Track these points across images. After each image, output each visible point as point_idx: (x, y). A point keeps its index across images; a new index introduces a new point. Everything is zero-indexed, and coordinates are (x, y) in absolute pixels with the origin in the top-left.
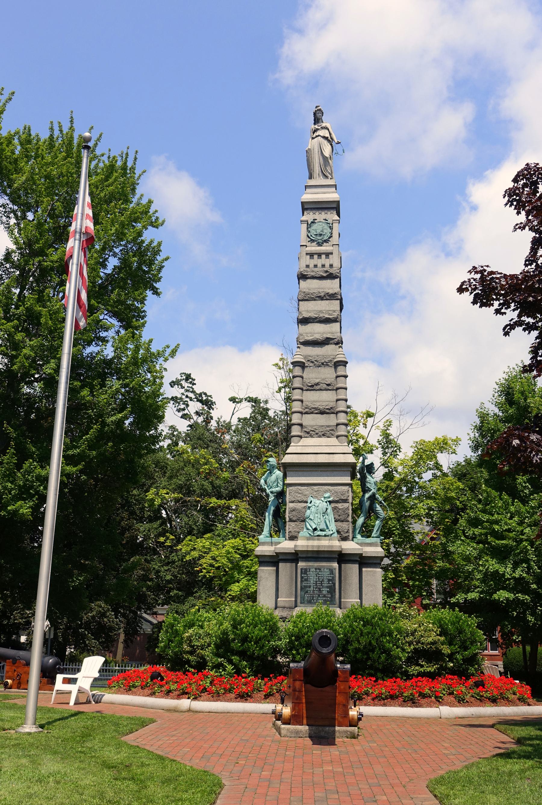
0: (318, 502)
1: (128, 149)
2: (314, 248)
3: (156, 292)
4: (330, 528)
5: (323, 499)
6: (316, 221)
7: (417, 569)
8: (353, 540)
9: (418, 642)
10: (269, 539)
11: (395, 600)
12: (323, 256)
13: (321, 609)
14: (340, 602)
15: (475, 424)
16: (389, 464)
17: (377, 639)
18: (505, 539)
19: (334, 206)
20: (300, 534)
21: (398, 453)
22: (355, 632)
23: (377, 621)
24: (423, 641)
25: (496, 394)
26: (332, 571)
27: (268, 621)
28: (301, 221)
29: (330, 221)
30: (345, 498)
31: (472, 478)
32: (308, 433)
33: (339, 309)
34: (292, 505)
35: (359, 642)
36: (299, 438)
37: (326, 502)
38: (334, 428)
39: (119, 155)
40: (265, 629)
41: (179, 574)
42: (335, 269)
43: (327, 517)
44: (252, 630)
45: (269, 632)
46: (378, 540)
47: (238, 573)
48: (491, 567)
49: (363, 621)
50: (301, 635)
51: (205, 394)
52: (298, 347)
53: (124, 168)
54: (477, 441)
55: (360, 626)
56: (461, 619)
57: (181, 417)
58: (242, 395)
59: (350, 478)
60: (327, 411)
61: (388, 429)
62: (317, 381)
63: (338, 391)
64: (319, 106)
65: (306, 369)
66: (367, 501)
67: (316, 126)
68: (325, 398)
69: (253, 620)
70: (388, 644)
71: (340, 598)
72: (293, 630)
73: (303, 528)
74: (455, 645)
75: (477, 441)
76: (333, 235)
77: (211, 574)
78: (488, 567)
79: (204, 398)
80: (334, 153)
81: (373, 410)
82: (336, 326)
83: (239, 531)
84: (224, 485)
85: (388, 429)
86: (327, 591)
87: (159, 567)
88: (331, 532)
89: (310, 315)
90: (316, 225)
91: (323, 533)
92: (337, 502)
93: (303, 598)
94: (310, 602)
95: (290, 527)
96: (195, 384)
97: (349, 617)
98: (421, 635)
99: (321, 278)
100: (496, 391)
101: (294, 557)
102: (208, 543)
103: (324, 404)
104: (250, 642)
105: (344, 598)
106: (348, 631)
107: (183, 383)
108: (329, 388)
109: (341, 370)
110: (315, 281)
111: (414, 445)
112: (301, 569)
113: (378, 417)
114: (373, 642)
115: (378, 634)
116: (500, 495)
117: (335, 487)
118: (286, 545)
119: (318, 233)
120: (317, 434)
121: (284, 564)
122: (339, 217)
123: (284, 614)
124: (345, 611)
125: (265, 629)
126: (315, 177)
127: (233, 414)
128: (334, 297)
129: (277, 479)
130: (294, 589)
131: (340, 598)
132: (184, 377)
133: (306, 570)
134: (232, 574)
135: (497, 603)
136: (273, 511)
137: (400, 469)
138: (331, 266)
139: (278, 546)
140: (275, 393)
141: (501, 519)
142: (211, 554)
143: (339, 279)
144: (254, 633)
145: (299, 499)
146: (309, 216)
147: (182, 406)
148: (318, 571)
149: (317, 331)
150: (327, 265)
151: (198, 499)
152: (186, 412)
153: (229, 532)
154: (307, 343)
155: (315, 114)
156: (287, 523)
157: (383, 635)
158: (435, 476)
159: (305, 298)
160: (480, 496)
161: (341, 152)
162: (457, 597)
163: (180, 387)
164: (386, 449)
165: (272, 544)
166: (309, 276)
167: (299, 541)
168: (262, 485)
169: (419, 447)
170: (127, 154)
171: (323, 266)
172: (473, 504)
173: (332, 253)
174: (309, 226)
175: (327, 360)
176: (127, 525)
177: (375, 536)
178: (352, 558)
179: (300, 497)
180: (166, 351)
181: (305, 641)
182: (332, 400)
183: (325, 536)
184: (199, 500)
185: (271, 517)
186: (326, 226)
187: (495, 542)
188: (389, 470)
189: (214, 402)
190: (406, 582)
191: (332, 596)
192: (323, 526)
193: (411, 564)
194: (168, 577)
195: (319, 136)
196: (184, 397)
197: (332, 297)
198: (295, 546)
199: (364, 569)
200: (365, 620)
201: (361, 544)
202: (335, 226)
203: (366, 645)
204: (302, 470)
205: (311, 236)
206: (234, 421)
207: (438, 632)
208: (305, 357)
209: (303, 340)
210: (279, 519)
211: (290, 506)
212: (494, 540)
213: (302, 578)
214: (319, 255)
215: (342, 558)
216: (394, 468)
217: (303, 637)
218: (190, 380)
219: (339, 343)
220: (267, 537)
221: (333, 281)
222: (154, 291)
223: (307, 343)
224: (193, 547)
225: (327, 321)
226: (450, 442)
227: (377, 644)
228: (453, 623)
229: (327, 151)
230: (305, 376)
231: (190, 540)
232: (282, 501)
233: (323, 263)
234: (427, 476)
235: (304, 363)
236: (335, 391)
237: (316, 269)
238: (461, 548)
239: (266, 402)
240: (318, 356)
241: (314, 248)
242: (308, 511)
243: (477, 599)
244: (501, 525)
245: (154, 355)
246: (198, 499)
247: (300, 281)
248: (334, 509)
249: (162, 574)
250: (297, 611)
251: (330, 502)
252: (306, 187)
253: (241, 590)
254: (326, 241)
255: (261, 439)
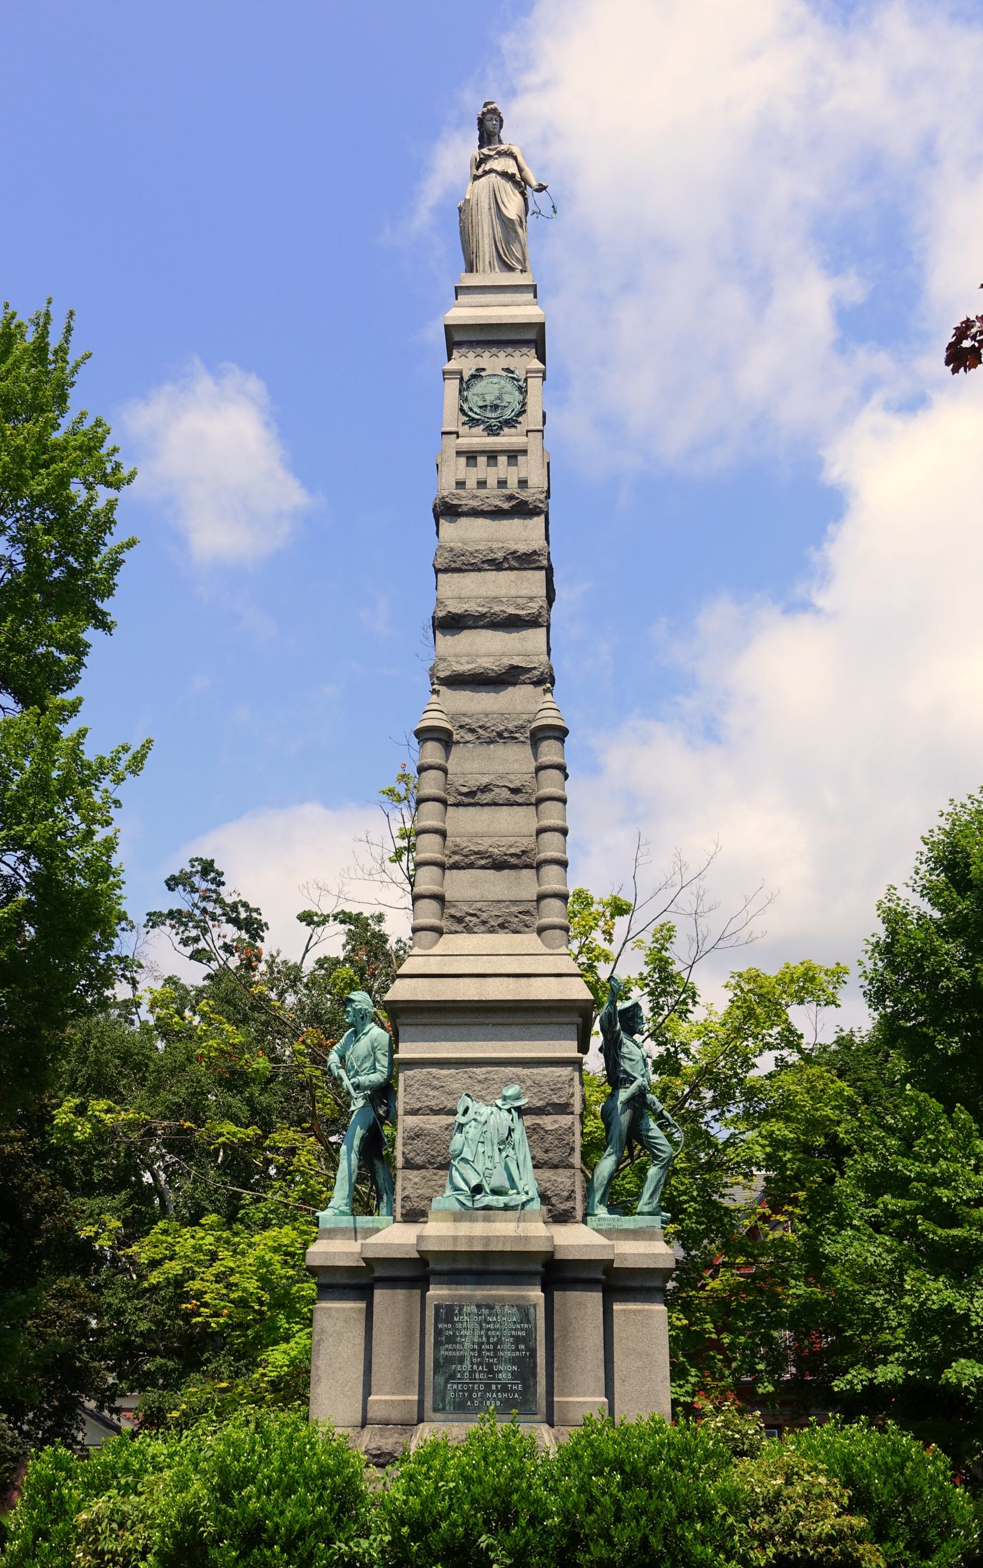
0: (485, 1110)
1: (49, 303)
2: (477, 439)
3: (103, 623)
4: (520, 1184)
5: (499, 1102)
6: (483, 374)
7: (739, 1305)
8: (584, 1222)
9: (789, 1535)
10: (347, 1221)
11: (688, 1387)
12: (502, 460)
13: (493, 1433)
14: (550, 1404)
15: (874, 940)
16: (669, 1035)
17: (665, 1530)
18: (962, 1227)
19: (532, 336)
20: (435, 1204)
21: (690, 1007)
22: (598, 1509)
23: (663, 1472)
24: (805, 1532)
25: (924, 868)
26: (525, 1313)
27: (330, 1474)
28: (444, 373)
29: (520, 374)
30: (563, 1100)
31: (860, 1079)
32: (460, 920)
33: (543, 592)
34: (411, 1121)
35: (609, 1540)
36: (434, 934)
37: (509, 1111)
38: (531, 907)
39: (31, 321)
40: (320, 1500)
41: (168, 1317)
42: (532, 491)
43: (511, 1153)
44: (276, 1505)
45: (330, 1510)
46: (656, 1221)
47: (288, 1318)
48: (934, 1297)
49: (622, 1472)
50: (428, 1519)
51: (245, 905)
52: (434, 692)
53: (41, 348)
54: (881, 981)
55: (614, 1489)
56: (909, 1458)
57: (191, 957)
58: (328, 907)
59: (575, 1044)
60: (513, 860)
61: (663, 948)
62: (485, 780)
63: (543, 806)
64: (492, 103)
65: (455, 750)
66: (623, 1112)
67: (485, 151)
68: (506, 827)
69: (282, 1471)
70: (700, 1548)
71: (550, 1393)
72: (405, 1502)
73: (443, 1186)
74: (894, 1540)
75: (881, 981)
76: (529, 408)
77: (222, 1320)
78: (927, 1299)
79: (243, 915)
80: (530, 212)
81: (626, 897)
82: (535, 637)
83: (296, 1208)
84: (278, 1106)
85: (663, 948)
86: (513, 1373)
87: (122, 1300)
88: (524, 1198)
89: (466, 607)
90: (484, 383)
91: (500, 1201)
92: (539, 1111)
93: (440, 1394)
94: (462, 1407)
95: (407, 1183)
96: (223, 884)
97: (577, 1457)
98: (797, 1513)
99: (497, 514)
100: (924, 859)
101: (417, 1272)
102: (210, 1239)
103: (504, 841)
104: (270, 1546)
105: (563, 1394)
106: (576, 1506)
107: (197, 880)
108: (519, 798)
109: (549, 752)
110: (480, 522)
111: (733, 982)
112: (437, 1308)
113: (641, 917)
114: (652, 1540)
115: (669, 1514)
116: (949, 1110)
117: (535, 1071)
118: (394, 1237)
119: (488, 403)
120: (484, 923)
121: (390, 1291)
122: (544, 363)
123: (387, 1442)
124: (568, 1435)
125: (320, 1500)
126: (481, 267)
127: (307, 950)
128: (530, 563)
129: (374, 1049)
130: (417, 1367)
131: (550, 1393)
132: (199, 868)
133: (450, 1309)
134: (273, 1319)
135: (954, 1394)
136: (362, 1139)
137: (695, 1046)
138: (523, 483)
139: (373, 1240)
140: (387, 862)
141: (956, 1173)
142: (218, 1267)
143: (542, 517)
144: (282, 1513)
145: (433, 1103)
146: (465, 362)
147: (194, 933)
148: (485, 1311)
149: (485, 649)
150: (513, 483)
151: (188, 1124)
152: (202, 944)
153: (271, 1212)
154: (457, 681)
155: (481, 122)
156: (400, 1174)
157: (685, 1516)
158: (782, 1064)
159: (453, 565)
160: (888, 1118)
161: (546, 210)
162: (849, 1377)
163: (188, 889)
164: (660, 996)
165: (355, 1233)
166: (465, 509)
167: (429, 1224)
168: (333, 1067)
169: (747, 987)
170: (47, 314)
171: (502, 483)
172: (877, 1138)
173: (524, 452)
174: (465, 384)
175: (511, 726)
176: (47, 1200)
177: (646, 1209)
178: (584, 1275)
179: (437, 1099)
180: (119, 759)
181: (443, 1540)
182: (528, 833)
183: (506, 1208)
184: (189, 1128)
185: (354, 1157)
186: (509, 386)
187: (935, 1233)
188: (668, 1050)
189: (266, 924)
190: (714, 1336)
191: (526, 1388)
192: (499, 1179)
193: (725, 1290)
194: (143, 1326)
195: (491, 171)
196: (197, 912)
197: (524, 561)
198: (420, 1238)
199: (617, 1307)
200: (628, 1469)
201: (607, 1233)
202: (534, 385)
203: (631, 1550)
204: (443, 1021)
205: (471, 409)
206: (309, 966)
207: (845, 1501)
208: (453, 717)
209: (448, 673)
210: (378, 1164)
211: (407, 1122)
212: (932, 1227)
213: (438, 1333)
214: (492, 456)
215: (556, 1273)
216: (682, 1043)
217: (436, 1526)
218: (213, 875)
219: (545, 680)
220: (343, 1213)
221: (527, 522)
222: (97, 620)
223: (457, 681)
224: (177, 1249)
225: (512, 623)
226: (822, 977)
227: (665, 1545)
228: (887, 1472)
229: (512, 206)
230: (451, 766)
231: (165, 1232)
232: (387, 1112)
233: (502, 476)
234: (765, 1063)
235: (449, 733)
236: (533, 808)
237: (482, 493)
238: (858, 1247)
239: (380, 918)
240: (487, 715)
241: (477, 439)
242: (458, 1136)
243: (900, 1381)
244: (956, 1188)
245: (90, 768)
246: (188, 1124)
247: (442, 521)
248: (532, 1131)
249: (127, 1318)
250: (426, 1433)
251: (521, 1111)
252: (458, 290)
253: (292, 1362)
254: (510, 423)
255: (352, 980)
